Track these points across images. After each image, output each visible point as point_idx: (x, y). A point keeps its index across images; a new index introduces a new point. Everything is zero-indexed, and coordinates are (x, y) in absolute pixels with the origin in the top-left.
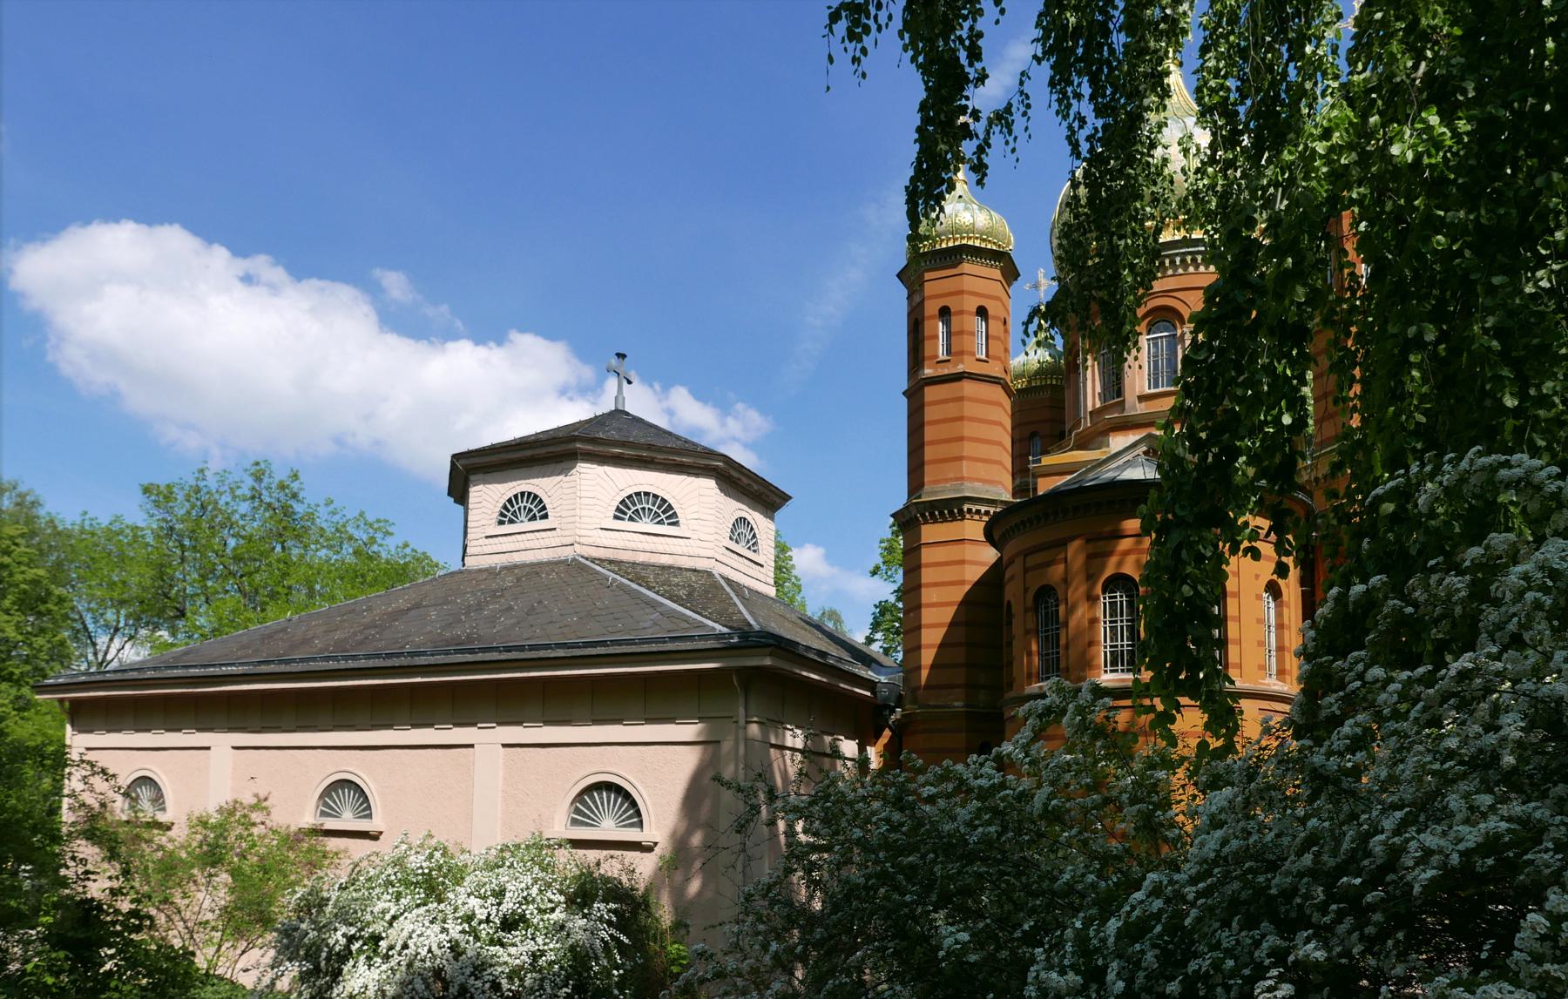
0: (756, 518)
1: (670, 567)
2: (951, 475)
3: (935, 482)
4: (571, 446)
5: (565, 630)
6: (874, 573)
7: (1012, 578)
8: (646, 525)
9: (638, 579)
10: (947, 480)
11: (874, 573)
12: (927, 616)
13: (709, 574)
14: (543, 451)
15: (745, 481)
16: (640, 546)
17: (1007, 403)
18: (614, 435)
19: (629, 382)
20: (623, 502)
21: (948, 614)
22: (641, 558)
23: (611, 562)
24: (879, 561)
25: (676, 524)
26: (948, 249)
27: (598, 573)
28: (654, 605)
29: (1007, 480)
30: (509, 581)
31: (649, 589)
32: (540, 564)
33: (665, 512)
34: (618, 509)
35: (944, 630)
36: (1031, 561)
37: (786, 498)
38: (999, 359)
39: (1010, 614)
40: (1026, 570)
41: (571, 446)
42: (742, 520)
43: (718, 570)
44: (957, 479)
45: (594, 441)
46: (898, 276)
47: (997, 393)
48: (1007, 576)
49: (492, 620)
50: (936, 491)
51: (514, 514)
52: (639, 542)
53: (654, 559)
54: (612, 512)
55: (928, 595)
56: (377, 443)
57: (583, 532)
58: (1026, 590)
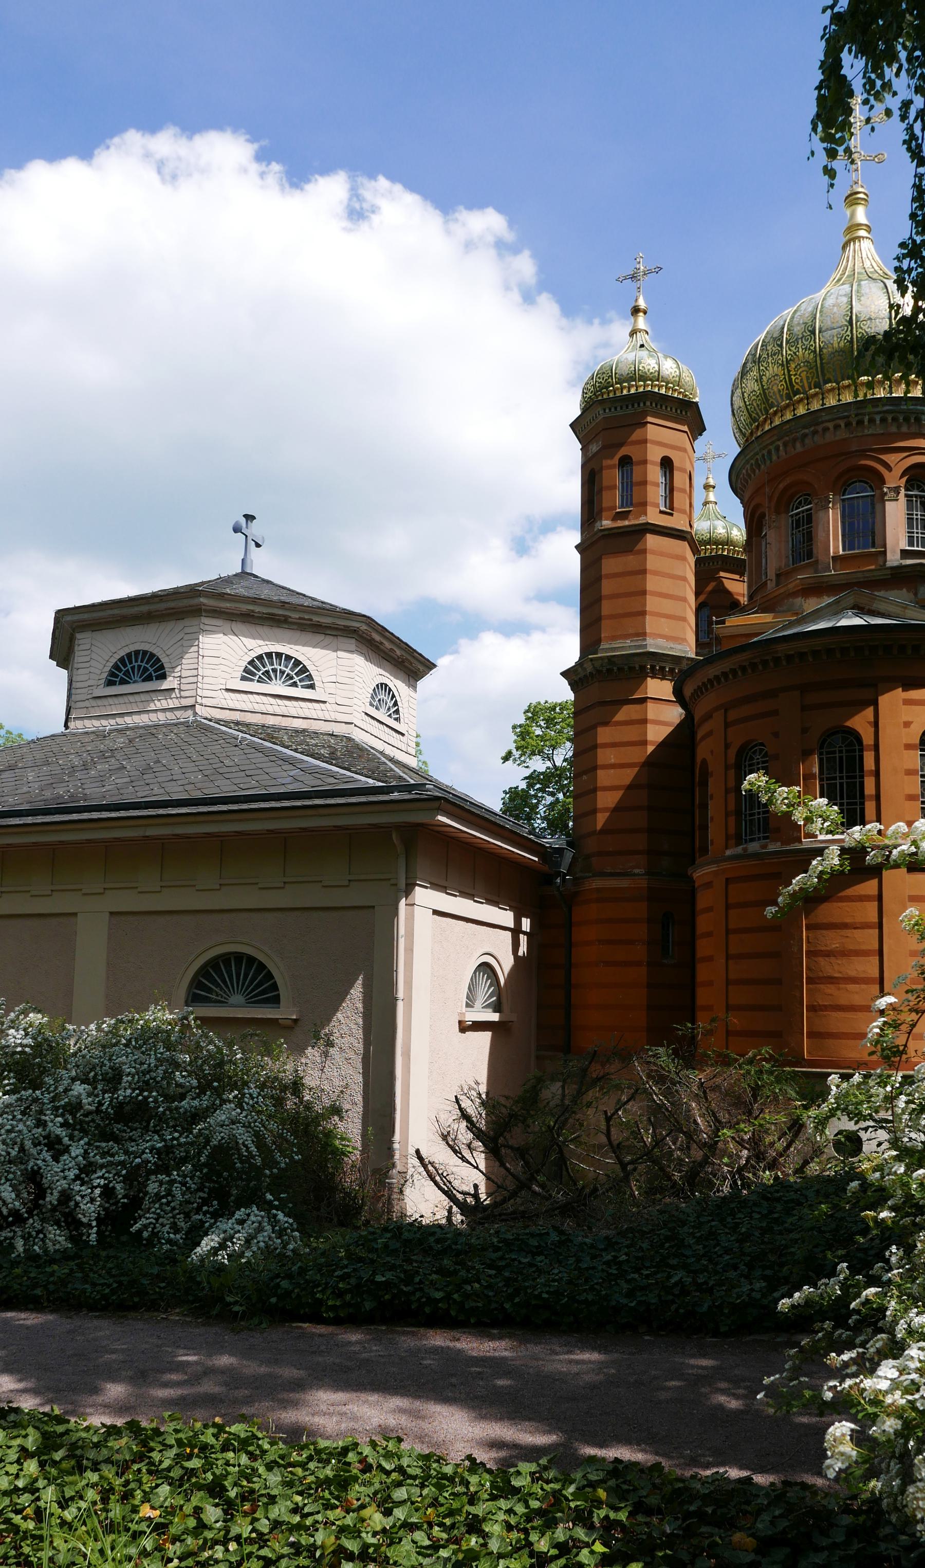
0: (398, 685)
1: (304, 730)
2: (631, 631)
3: (614, 638)
4: (195, 601)
5: (187, 787)
6: (506, 758)
7: (710, 734)
8: (278, 687)
9: (271, 738)
10: (626, 636)
11: (506, 758)
12: (604, 777)
13: (349, 739)
14: (162, 606)
15: (388, 645)
16: (270, 710)
17: (691, 559)
18: (242, 591)
19: (258, 545)
20: (251, 663)
21: (628, 776)
22: (271, 721)
23: (237, 723)
24: (512, 747)
25: (312, 686)
26: (630, 396)
27: (224, 733)
28: (292, 762)
29: (691, 638)
30: (121, 741)
31: (287, 747)
32: (156, 726)
33: (302, 674)
34: (246, 670)
35: (620, 793)
36: (733, 715)
37: (435, 666)
38: (683, 512)
39: (705, 773)
40: (727, 725)
41: (195, 601)
42: (383, 686)
43: (359, 736)
44: (637, 635)
45: (222, 596)
46: (571, 425)
47: (684, 548)
48: (699, 735)
49: (101, 780)
50: (616, 646)
51: (127, 673)
52: (267, 704)
53: (285, 723)
54: (239, 672)
55: (605, 756)
56: (108, 148)
57: (206, 693)
58: (727, 746)
